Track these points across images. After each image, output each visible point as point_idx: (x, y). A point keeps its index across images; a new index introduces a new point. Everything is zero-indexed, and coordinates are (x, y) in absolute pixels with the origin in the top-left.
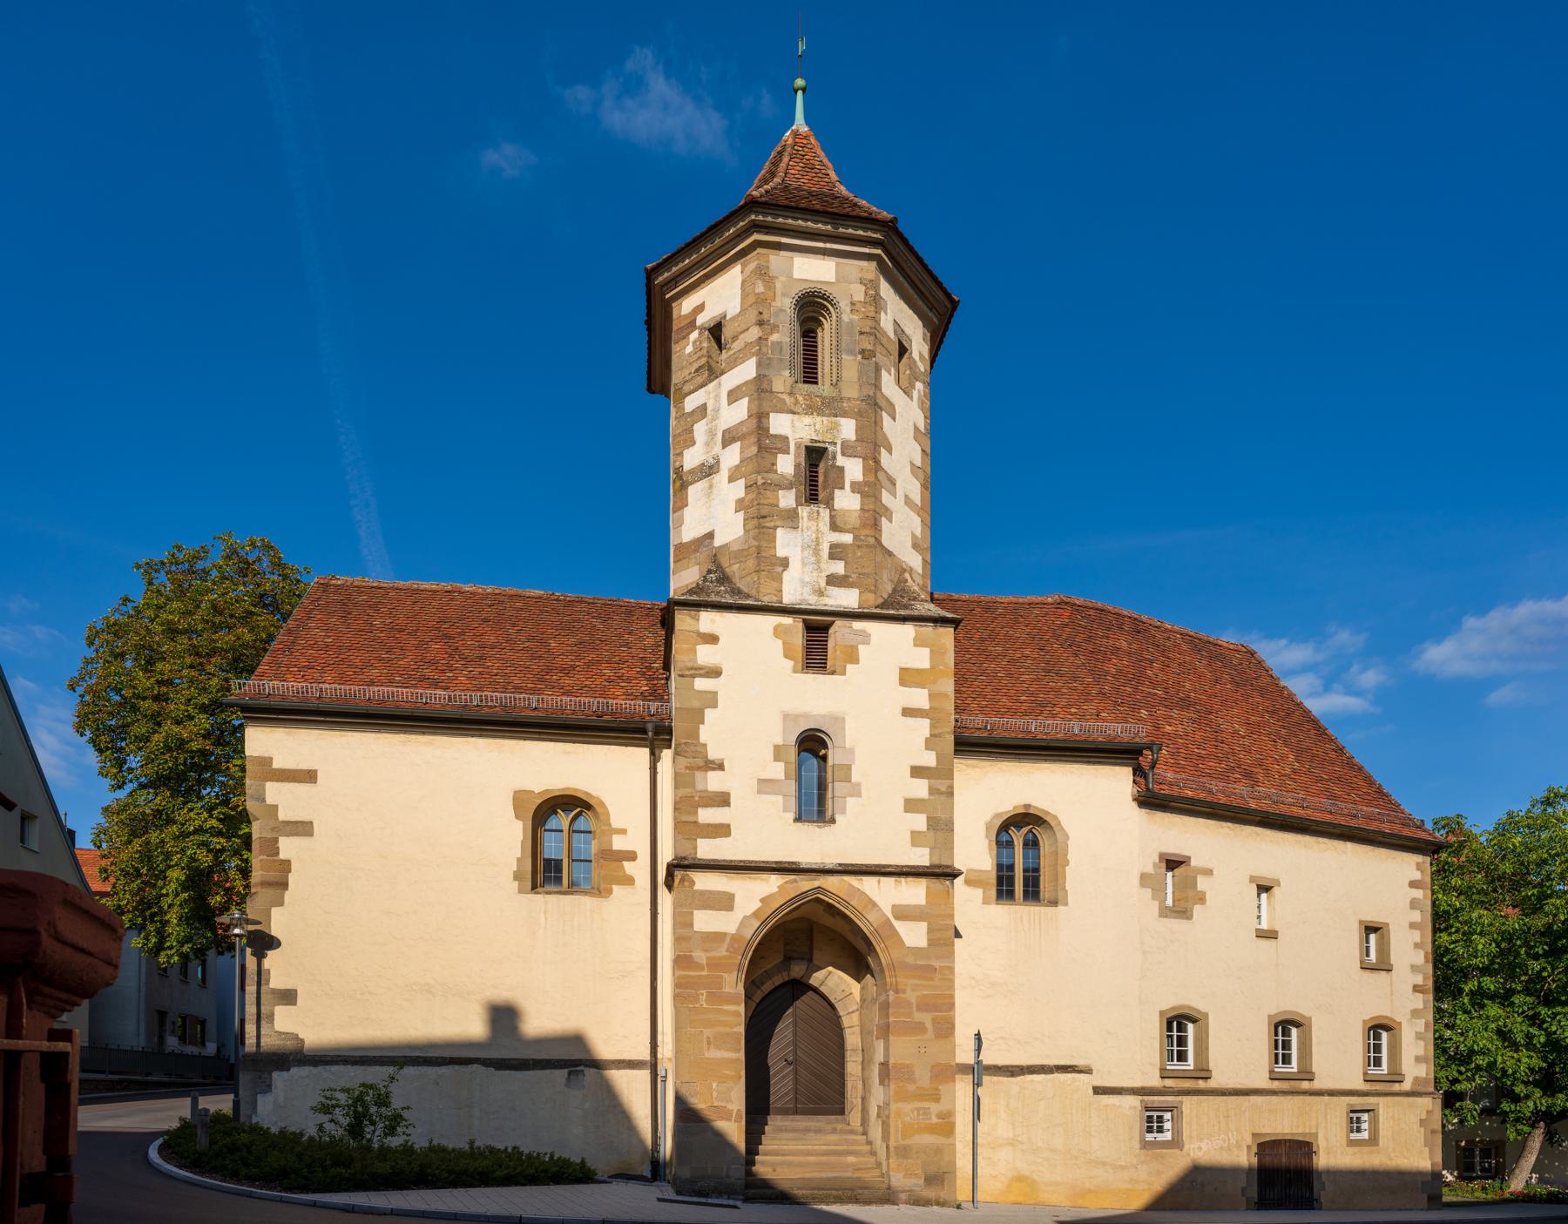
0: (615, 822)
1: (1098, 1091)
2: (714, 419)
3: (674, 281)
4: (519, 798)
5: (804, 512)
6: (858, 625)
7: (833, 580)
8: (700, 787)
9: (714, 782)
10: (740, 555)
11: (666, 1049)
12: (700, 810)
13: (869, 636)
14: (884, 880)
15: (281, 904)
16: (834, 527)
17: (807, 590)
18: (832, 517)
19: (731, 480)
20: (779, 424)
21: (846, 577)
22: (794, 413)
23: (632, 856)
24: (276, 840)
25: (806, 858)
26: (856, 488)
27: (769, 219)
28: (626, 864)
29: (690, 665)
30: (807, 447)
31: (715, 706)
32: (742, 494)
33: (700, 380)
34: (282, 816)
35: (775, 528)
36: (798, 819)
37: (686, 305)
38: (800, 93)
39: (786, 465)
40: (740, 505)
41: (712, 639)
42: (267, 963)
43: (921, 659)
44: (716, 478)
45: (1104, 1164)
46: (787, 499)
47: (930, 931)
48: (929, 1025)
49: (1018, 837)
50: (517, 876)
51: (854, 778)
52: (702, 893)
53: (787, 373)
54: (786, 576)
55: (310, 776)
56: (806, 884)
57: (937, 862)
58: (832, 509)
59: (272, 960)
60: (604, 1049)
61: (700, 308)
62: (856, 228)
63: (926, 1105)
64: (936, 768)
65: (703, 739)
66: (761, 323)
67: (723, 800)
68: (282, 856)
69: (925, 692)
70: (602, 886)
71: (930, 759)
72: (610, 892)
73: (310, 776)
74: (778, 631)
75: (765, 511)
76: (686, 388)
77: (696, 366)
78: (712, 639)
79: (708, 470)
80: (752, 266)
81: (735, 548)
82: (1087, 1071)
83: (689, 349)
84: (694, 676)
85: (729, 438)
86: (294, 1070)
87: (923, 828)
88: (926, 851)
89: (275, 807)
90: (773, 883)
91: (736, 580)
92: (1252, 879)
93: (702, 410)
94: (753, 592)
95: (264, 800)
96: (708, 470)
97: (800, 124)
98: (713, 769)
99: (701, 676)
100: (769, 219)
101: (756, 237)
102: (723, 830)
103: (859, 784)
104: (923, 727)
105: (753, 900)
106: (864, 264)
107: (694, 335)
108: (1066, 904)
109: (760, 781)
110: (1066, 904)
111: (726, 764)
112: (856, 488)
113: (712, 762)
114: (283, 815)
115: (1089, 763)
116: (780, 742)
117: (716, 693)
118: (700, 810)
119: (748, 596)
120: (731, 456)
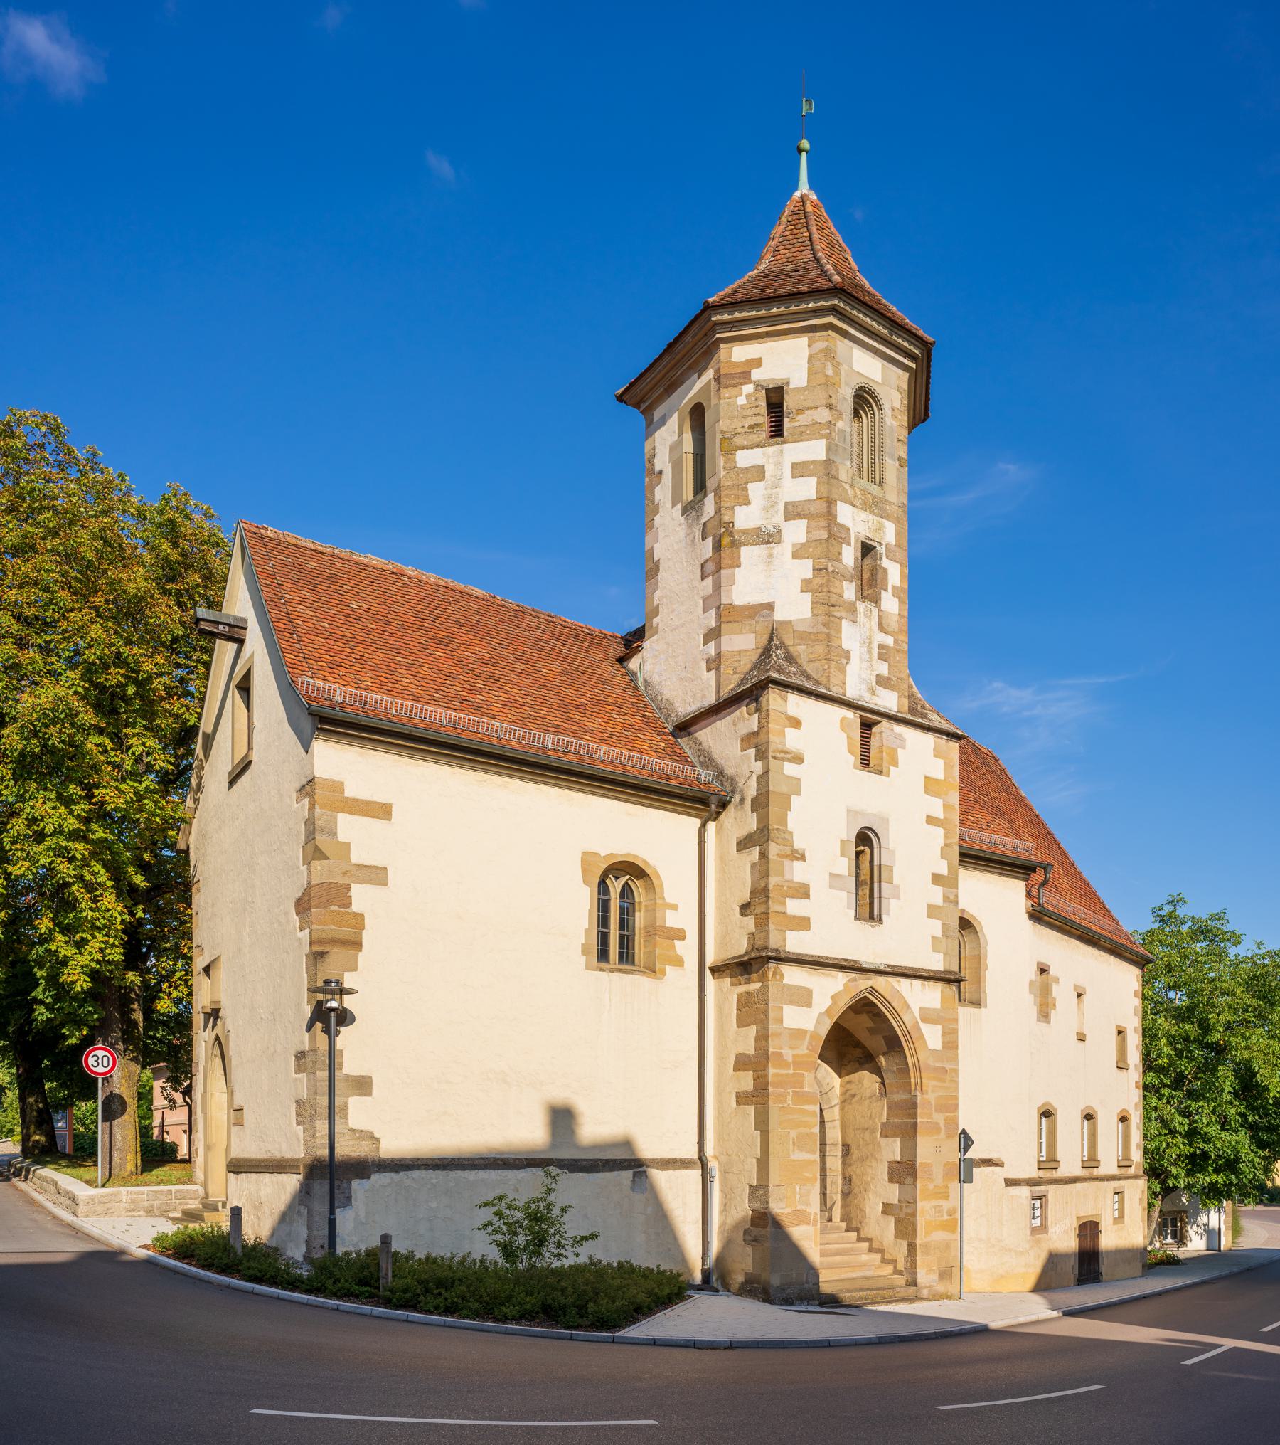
1: (1010, 1182)
2: (774, 486)
3: (732, 324)
4: (587, 859)
5: (861, 606)
6: (899, 729)
7: (882, 681)
8: (787, 877)
9: (798, 872)
10: (804, 637)
11: (709, 1150)
13: (904, 740)
14: (915, 982)
15: (355, 969)
17: (864, 687)
18: (880, 617)
19: (796, 556)
20: (845, 514)
21: (889, 679)
23: (681, 935)
24: (348, 887)
25: (866, 959)
26: (840, 575)
27: (847, 308)
29: (780, 747)
31: (799, 794)
32: (809, 575)
34: (355, 858)
35: (841, 618)
36: (857, 918)
37: (740, 353)
38: (804, 155)
40: (806, 586)
41: (796, 723)
42: (340, 1042)
43: (937, 769)
44: (777, 549)
45: (1010, 1250)
46: (849, 591)
47: (944, 1034)
48: (942, 1125)
49: (615, 887)
50: (585, 951)
51: (895, 881)
52: (790, 987)
53: (848, 463)
55: (382, 811)
56: (863, 983)
58: (880, 610)
59: (345, 1038)
60: (647, 1150)
61: (758, 363)
62: (905, 339)
63: (940, 1202)
65: (790, 826)
68: (355, 908)
69: (940, 802)
70: (658, 966)
71: (943, 869)
72: (664, 973)
73: (382, 811)
74: (844, 723)
75: (833, 600)
76: (738, 441)
78: (796, 723)
79: (768, 538)
80: (820, 345)
81: (801, 628)
82: (999, 1164)
83: (742, 401)
84: (783, 760)
85: (793, 511)
86: (375, 1177)
87: (939, 934)
88: (941, 956)
89: (347, 846)
90: (839, 980)
91: (802, 660)
92: (1076, 987)
94: (823, 680)
95: (335, 835)
96: (768, 538)
97: (804, 188)
98: (798, 859)
99: (789, 760)
100: (847, 308)
101: (831, 319)
102: (802, 923)
103: (898, 887)
106: (901, 372)
107: (748, 388)
109: (832, 875)
112: (840, 575)
113: (796, 851)
114: (356, 857)
115: (1001, 874)
118: (788, 900)
119: (817, 683)
120: (796, 532)
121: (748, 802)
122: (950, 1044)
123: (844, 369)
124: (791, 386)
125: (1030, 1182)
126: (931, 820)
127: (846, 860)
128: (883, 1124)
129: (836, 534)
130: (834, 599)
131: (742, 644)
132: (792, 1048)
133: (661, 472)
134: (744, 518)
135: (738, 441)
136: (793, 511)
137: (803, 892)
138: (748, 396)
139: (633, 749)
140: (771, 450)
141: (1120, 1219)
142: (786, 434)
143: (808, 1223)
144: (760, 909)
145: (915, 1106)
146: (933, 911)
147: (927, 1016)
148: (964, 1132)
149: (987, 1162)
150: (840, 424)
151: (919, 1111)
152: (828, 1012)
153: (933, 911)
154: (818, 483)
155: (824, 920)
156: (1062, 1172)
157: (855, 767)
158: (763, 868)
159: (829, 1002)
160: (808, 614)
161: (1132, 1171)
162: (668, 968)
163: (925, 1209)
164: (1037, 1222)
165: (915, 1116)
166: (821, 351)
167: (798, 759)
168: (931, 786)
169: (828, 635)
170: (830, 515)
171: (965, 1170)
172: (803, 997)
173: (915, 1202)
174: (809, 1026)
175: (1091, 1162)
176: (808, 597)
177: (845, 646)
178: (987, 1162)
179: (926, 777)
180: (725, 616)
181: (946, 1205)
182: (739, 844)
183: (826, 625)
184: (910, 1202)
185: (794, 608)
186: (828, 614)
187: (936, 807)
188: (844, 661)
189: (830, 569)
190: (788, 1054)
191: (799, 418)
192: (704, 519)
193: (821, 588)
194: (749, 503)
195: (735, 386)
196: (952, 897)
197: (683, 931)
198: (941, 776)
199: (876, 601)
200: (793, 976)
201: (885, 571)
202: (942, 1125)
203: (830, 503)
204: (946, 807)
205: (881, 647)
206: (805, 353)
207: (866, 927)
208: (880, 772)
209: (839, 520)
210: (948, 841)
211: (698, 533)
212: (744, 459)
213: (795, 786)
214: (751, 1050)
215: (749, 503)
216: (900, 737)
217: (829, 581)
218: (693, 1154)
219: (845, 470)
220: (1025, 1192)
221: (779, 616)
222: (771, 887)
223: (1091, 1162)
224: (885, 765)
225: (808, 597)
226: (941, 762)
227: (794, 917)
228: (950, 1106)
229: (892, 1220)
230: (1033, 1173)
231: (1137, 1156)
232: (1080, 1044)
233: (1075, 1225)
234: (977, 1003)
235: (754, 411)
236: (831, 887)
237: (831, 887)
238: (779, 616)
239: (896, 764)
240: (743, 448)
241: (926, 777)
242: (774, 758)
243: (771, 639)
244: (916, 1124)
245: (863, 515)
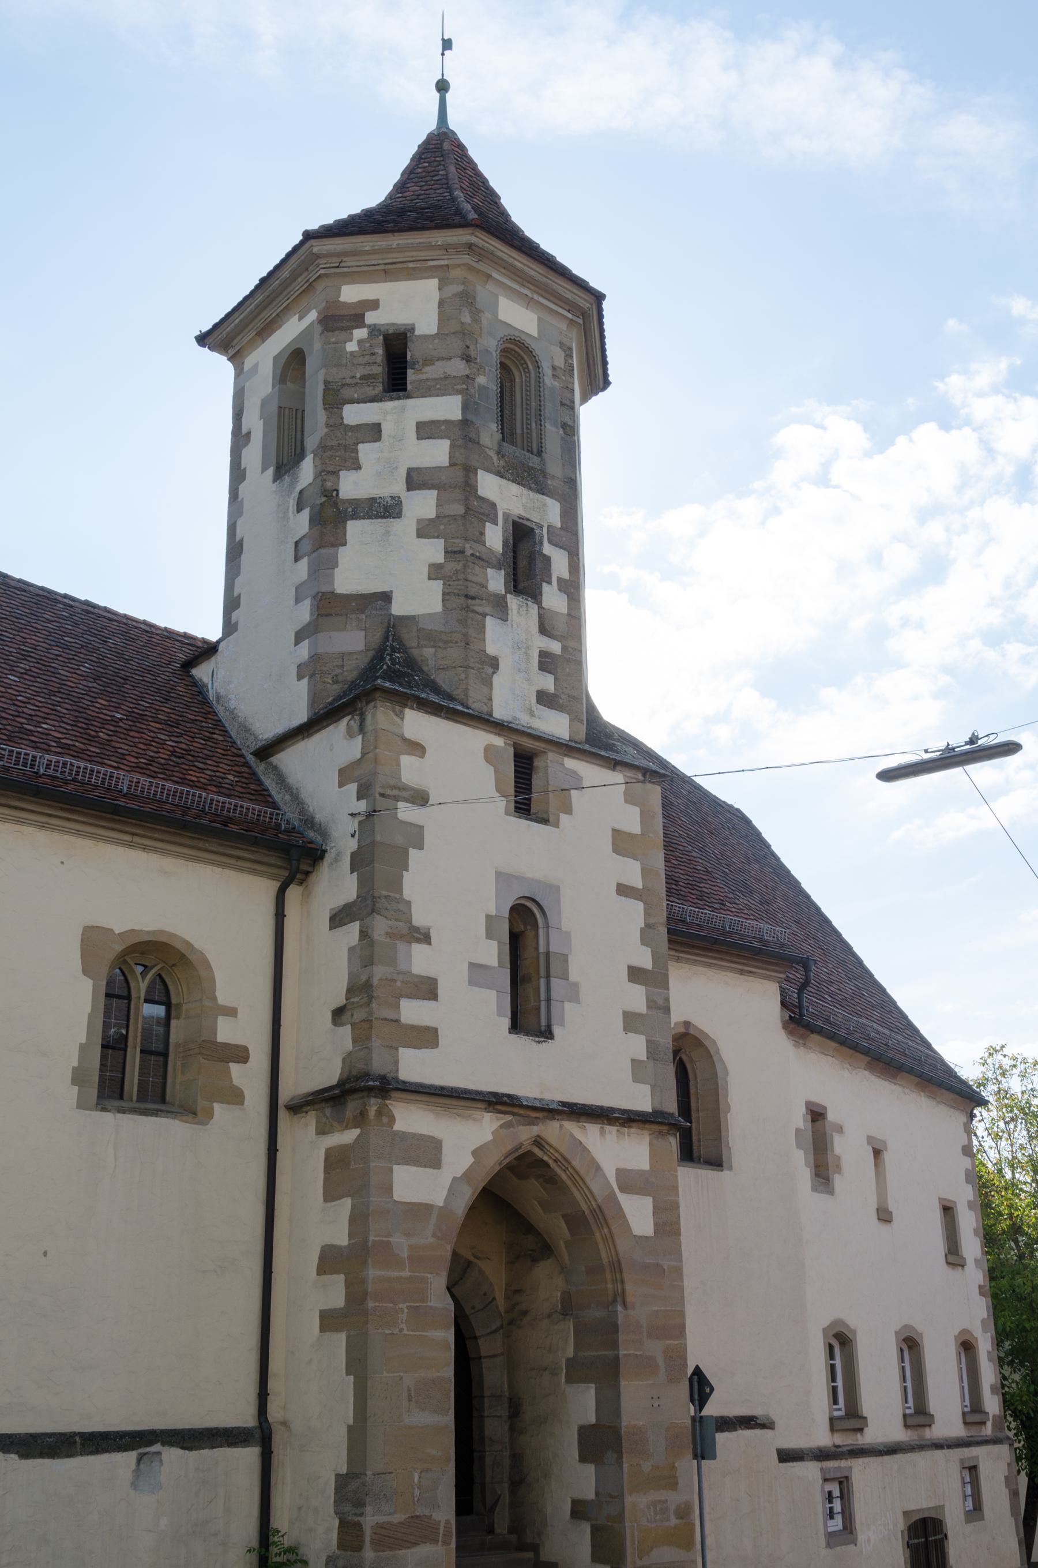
0: (224, 996)
1: (786, 1456)
4: (92, 938)
5: (513, 602)
9: (420, 960)
12: (404, 1003)
16: (544, 630)
18: (540, 616)
20: (490, 485)
21: (554, 696)
22: (502, 477)
23: (241, 1055)
25: (526, 1089)
26: (483, 560)
28: (235, 1068)
29: (392, 782)
30: (514, 523)
32: (440, 558)
33: (370, 391)
35: (484, 615)
39: (495, 538)
40: (435, 572)
41: (417, 749)
43: (631, 820)
44: (395, 524)
46: (496, 581)
47: (656, 1211)
48: (661, 1362)
50: (78, 1078)
52: (404, 1136)
54: (497, 680)
57: (658, 1108)
58: (540, 607)
61: (374, 305)
64: (652, 972)
66: (468, 359)
67: (427, 989)
69: (636, 866)
71: (644, 959)
72: (210, 1114)
76: (346, 393)
77: (366, 371)
78: (417, 749)
79: (386, 509)
83: (352, 347)
84: (397, 799)
85: (416, 480)
87: (642, 1055)
92: (870, 1140)
93: (374, 432)
96: (386, 509)
98: (418, 941)
99: (405, 800)
102: (426, 1037)
104: (635, 913)
105: (467, 1144)
107: (360, 333)
108: (730, 1168)
110: (730, 1168)
111: (433, 934)
112: (483, 560)
113: (417, 929)
115: (741, 972)
116: (493, 912)
117: (422, 827)
118: (404, 1003)
119: (451, 698)
120: (423, 505)
121: (347, 859)
122: (668, 1223)
123: (486, 317)
124: (417, 333)
125: (822, 1455)
126: (624, 890)
127: (495, 944)
128: (568, 1360)
129: (482, 511)
130: (473, 591)
131: (351, 642)
132: (408, 1235)
133: (249, 434)
134: (352, 486)
135: (346, 393)
136: (416, 480)
137: (427, 989)
138: (360, 342)
139: (183, 782)
140: (389, 405)
141: (976, 1511)
142: (409, 387)
143: (435, 1541)
144: (359, 1015)
145: (614, 1328)
146: (631, 1022)
147: (629, 1181)
148: (698, 1371)
149: (748, 1422)
150: (481, 380)
151: (621, 1337)
152: (468, 1176)
153: (631, 1022)
154: (452, 447)
155: (465, 1037)
156: (871, 1436)
157: (507, 813)
158: (366, 953)
159: (469, 1160)
160: (438, 608)
161: (988, 1430)
162: (216, 1106)
163: (639, 1505)
164: (837, 1524)
165: (614, 1345)
166: (455, 295)
167: (421, 798)
168: (622, 843)
169: (465, 635)
170: (469, 487)
171: (701, 1439)
172: (427, 1153)
173: (622, 1495)
174: (438, 1198)
175: (919, 1415)
176: (438, 586)
177: (491, 650)
178: (748, 1422)
179: (615, 831)
180: (330, 608)
181: (674, 1499)
182: (332, 919)
183: (462, 622)
184: (610, 1495)
185: (418, 598)
186: (467, 609)
187: (632, 873)
188: (490, 670)
189: (469, 552)
190: (401, 1244)
191: (427, 369)
192: (299, 487)
193: (456, 575)
194: (359, 467)
195: (343, 329)
196: (661, 1002)
197: (246, 1049)
198: (635, 828)
199: (535, 595)
200: (410, 1119)
201: (547, 560)
202: (661, 1362)
203: (469, 472)
204: (645, 872)
205: (543, 655)
206: (436, 297)
207: (524, 1043)
208: (544, 821)
209: (480, 493)
210: (651, 921)
211: (292, 503)
212: (354, 414)
213: (416, 836)
214: (342, 1239)
215: (359, 467)
216: (573, 774)
217: (465, 567)
218: (244, 1416)
219: (489, 433)
220: (810, 1471)
221: (397, 609)
222: (375, 982)
223: (919, 1415)
224: (552, 810)
225: (438, 586)
226: (637, 810)
227: (413, 1027)
228: (673, 1328)
229: (586, 1528)
230: (822, 1438)
231: (992, 1404)
232: (884, 1228)
233: (901, 1525)
234: (716, 1163)
235: (367, 359)
236: (471, 983)
237: (471, 983)
238: (397, 609)
239: (569, 811)
240: (352, 401)
241: (615, 831)
242: (382, 795)
243: (386, 638)
244: (617, 1359)
245: (515, 489)
